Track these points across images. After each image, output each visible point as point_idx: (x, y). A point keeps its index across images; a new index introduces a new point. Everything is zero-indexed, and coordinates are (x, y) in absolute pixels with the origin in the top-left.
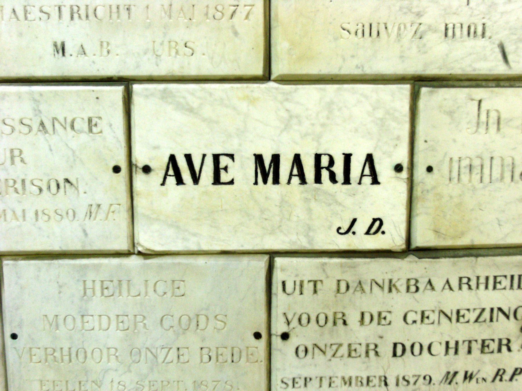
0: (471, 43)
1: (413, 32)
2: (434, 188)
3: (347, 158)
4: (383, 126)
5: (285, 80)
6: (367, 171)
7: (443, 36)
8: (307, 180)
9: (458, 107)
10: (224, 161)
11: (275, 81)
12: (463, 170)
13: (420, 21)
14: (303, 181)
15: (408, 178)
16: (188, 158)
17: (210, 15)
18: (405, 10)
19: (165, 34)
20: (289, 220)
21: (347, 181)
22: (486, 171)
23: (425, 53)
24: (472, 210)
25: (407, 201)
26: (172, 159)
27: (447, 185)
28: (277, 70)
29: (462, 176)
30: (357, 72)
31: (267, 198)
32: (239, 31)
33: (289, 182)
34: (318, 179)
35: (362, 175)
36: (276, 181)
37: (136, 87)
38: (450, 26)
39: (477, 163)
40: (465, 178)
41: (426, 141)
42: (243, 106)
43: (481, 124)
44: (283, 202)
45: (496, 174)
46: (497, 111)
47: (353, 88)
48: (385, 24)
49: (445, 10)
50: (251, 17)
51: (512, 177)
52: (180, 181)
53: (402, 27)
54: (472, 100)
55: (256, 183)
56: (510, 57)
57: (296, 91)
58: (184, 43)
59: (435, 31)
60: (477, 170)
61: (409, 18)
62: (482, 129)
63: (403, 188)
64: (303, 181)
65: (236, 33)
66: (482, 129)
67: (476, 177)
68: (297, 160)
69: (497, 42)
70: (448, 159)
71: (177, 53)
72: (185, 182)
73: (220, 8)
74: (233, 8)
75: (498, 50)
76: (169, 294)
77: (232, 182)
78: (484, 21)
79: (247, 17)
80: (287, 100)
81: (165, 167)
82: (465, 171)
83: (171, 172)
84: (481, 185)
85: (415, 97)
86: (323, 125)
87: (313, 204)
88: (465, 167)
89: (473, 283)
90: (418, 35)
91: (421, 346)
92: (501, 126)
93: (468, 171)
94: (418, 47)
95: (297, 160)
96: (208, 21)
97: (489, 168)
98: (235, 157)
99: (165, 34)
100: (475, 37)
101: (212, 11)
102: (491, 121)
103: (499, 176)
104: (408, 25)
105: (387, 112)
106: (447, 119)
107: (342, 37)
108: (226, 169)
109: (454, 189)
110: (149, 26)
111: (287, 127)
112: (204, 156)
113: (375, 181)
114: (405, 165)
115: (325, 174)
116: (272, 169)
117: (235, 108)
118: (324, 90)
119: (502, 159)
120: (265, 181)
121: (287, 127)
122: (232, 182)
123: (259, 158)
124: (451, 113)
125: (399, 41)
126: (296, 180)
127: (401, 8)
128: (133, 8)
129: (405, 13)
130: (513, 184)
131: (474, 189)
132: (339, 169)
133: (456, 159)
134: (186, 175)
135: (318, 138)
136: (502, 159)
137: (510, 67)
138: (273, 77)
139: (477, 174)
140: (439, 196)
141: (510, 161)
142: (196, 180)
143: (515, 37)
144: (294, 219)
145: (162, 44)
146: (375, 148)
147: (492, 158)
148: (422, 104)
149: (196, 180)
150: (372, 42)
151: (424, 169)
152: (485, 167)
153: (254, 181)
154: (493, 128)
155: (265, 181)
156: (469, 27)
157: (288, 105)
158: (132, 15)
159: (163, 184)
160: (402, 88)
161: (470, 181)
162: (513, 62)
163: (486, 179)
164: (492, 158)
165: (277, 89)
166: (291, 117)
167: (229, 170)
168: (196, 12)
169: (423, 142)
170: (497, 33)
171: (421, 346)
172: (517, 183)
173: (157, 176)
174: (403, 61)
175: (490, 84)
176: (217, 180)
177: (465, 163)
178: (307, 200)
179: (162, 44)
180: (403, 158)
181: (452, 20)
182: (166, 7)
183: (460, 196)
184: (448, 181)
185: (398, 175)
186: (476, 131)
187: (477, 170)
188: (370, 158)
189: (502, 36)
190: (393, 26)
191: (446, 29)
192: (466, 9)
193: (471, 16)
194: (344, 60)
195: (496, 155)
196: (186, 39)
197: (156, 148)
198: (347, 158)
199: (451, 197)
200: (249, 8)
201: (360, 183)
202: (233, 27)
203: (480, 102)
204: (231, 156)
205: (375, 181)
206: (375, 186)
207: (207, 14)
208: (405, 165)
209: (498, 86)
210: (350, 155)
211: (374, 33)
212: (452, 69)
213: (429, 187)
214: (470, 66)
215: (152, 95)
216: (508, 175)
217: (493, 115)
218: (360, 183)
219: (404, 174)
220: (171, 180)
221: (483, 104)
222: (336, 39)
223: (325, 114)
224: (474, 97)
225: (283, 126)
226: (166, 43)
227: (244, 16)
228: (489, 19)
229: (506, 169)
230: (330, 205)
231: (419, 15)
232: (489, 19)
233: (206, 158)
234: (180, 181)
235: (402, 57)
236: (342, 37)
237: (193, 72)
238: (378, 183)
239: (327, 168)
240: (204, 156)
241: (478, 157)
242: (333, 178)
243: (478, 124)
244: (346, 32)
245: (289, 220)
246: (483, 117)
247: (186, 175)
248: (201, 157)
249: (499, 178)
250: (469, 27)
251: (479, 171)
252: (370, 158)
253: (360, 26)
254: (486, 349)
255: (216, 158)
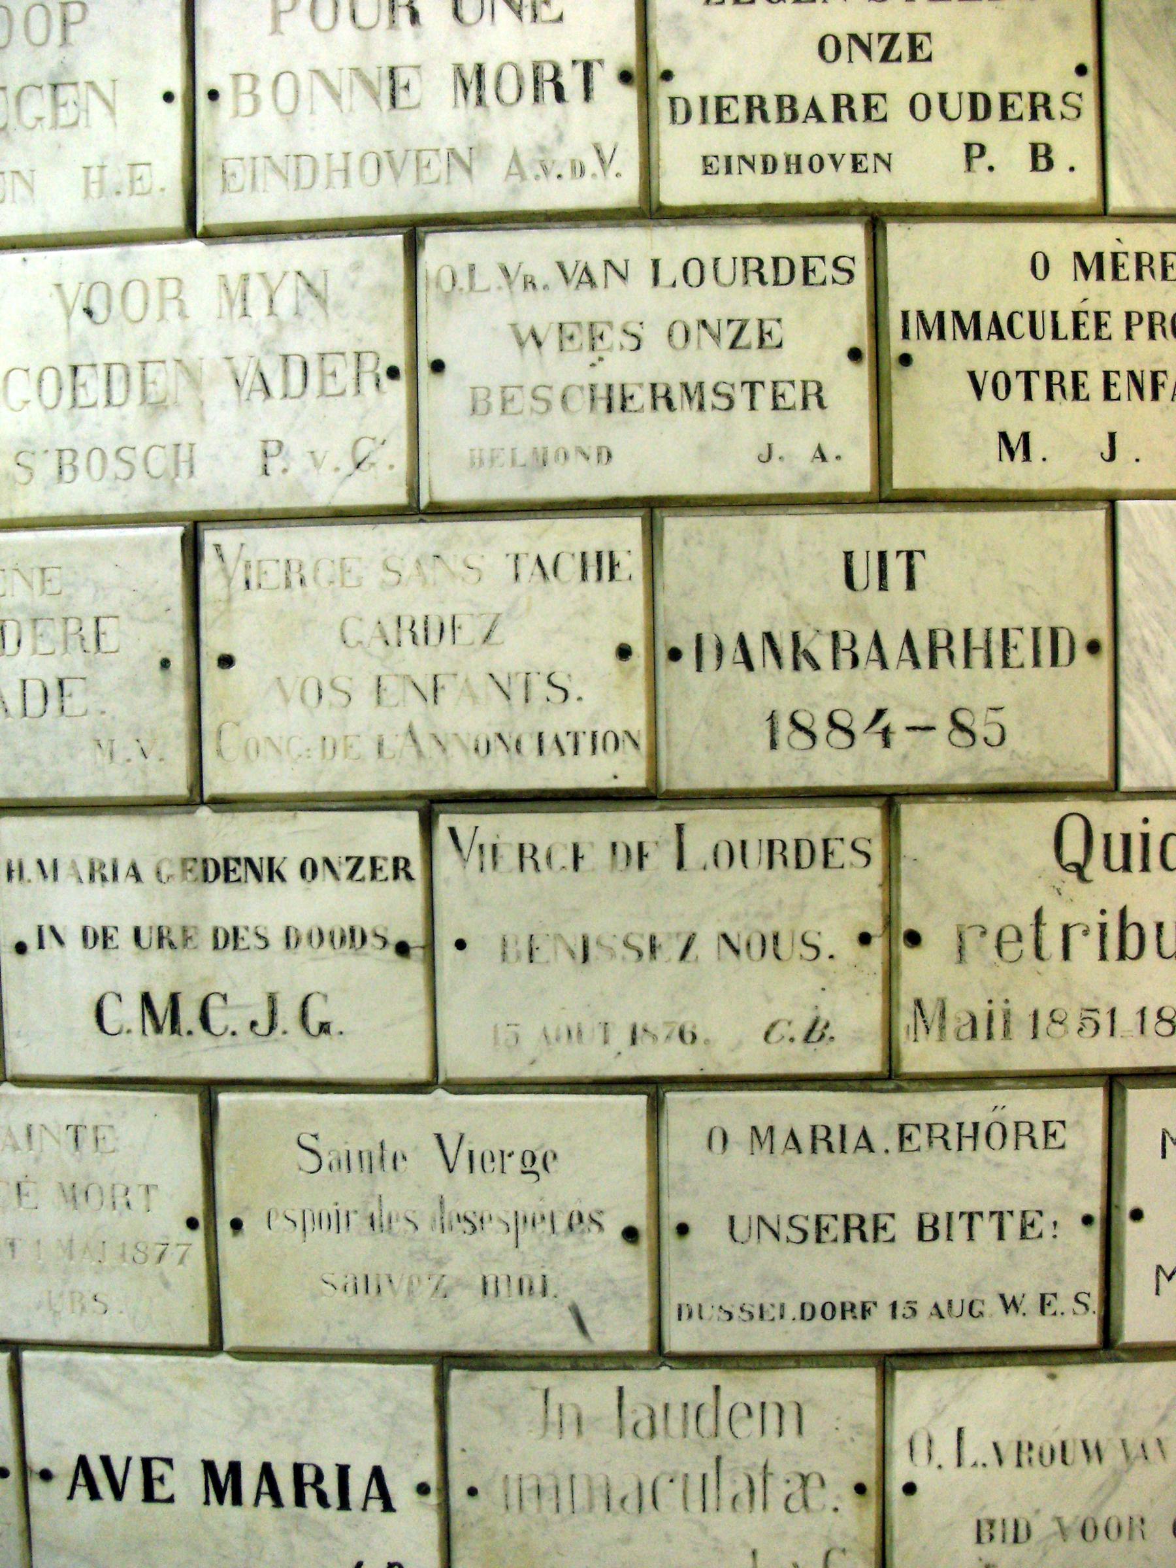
0: (526, 1305)
1: (433, 1288)
2: (481, 1519)
3: (343, 1472)
4: (394, 1425)
5: (242, 1354)
6: (374, 1491)
7: (481, 1294)
8: (284, 1501)
9: (512, 1400)
10: (158, 1469)
11: (229, 1352)
12: (525, 1494)
13: (442, 1272)
14: (278, 1502)
15: (439, 1504)
16: (106, 1461)
17: (128, 1258)
18: (419, 1256)
19: (65, 1282)
20: (259, 1559)
21: (344, 1504)
22: (565, 1495)
23: (453, 1318)
24: (546, 1554)
25: (440, 1539)
26: (83, 1461)
27: (502, 1516)
28: (233, 1337)
29: (526, 1503)
30: (350, 1346)
31: (225, 1526)
32: (172, 1280)
33: (256, 1503)
34: (300, 1501)
35: (367, 1498)
36: (237, 1500)
37: (27, 1356)
38: (491, 1280)
39: (548, 1483)
40: (530, 1505)
41: (463, 1450)
42: (183, 1390)
43: (550, 1426)
44: (250, 1532)
45: (581, 1498)
46: (576, 1406)
47: (345, 1369)
48: (389, 1276)
49: (481, 1255)
50: (186, 1260)
51: (608, 1504)
52: (95, 1495)
53: (415, 1281)
54: (533, 1389)
55: (207, 1502)
56: (588, 1326)
57: (258, 1370)
58: (92, 1295)
59: (468, 1286)
60: (549, 1494)
61: (425, 1267)
62: (553, 1433)
63: (431, 1521)
64: (278, 1502)
65: (166, 1284)
66: (553, 1433)
67: (548, 1505)
68: (267, 1471)
69: (568, 1303)
70: (500, 1478)
71: (83, 1308)
72: (102, 1494)
73: (141, 1247)
74: (162, 1248)
75: (568, 1315)
76: (48, 121)
77: (171, 1500)
78: (544, 1271)
79: (181, 1262)
80: (246, 1383)
81: (72, 1473)
82: (530, 1495)
83: (81, 1480)
84: (557, 1517)
85: (442, 1383)
86: (302, 1422)
87: (296, 1539)
88: (529, 1490)
89: (952, 1138)
90: (441, 1293)
91: (813, 1308)
92: (584, 1428)
93: (535, 1495)
94: (442, 1311)
95: (267, 1471)
96: (125, 1264)
97: (569, 1491)
98: (174, 1462)
99: (65, 1282)
100: (530, 1294)
101: (130, 1252)
102: (566, 1421)
103: (586, 1503)
104: (425, 1278)
105: (400, 1406)
106: (496, 1418)
107: (322, 1294)
108: (161, 1479)
109: (513, 1522)
110: (42, 1269)
111: (249, 1422)
112: (129, 1459)
113: (388, 1507)
114: (433, 1484)
115: (310, 1494)
116: (230, 1483)
117: (169, 1392)
118: (300, 1370)
119: (590, 1479)
120: (221, 1501)
121: (249, 1422)
122: (171, 1500)
123: (209, 1467)
124: (500, 1409)
125: (411, 1302)
126: (266, 1501)
127: (411, 1254)
128: (18, 1244)
129: (419, 1260)
130: (610, 1515)
131: (546, 1523)
132: (330, 1485)
133: (513, 1477)
134: (104, 1487)
135: (296, 1440)
136: (590, 1479)
137: (591, 1341)
138: (226, 1347)
139: (550, 1500)
140: (491, 1533)
141: (601, 1480)
142: (118, 1494)
143: (595, 1296)
144: (268, 1558)
145: (61, 1295)
146: (385, 1458)
147: (572, 1476)
148: (453, 1394)
149: (118, 1494)
150: (370, 1301)
151: (464, 1491)
152: (561, 1488)
153: (203, 1499)
154: (570, 1432)
155: (221, 1501)
156: (521, 1280)
157: (249, 1391)
158: (17, 1254)
159: (71, 1497)
160: (419, 1371)
161: (539, 1510)
162: (597, 1332)
163: (566, 1506)
164: (572, 1476)
165: (231, 1366)
166: (254, 1408)
167: (166, 1481)
168: (107, 1252)
169: (459, 1450)
170: (566, 1289)
171: (813, 1308)
172: (616, 1514)
173: (61, 1485)
174: (419, 1331)
175: (562, 1364)
176: (149, 1496)
177: (529, 1483)
178: (285, 1531)
179: (61, 1295)
180: (428, 1471)
181: (491, 1272)
182: (65, 1242)
183: (524, 1532)
184: (502, 1510)
185: (424, 1499)
186: (543, 1436)
187: (549, 1494)
188: (377, 1473)
189: (574, 1294)
190: (401, 1280)
191: (485, 1283)
192: (513, 1254)
193: (523, 1264)
194: (328, 1327)
195: (577, 1471)
196: (95, 1291)
197: (58, 1444)
198: (343, 1472)
199: (510, 1534)
200: (184, 1248)
201: (364, 1509)
202: (162, 1274)
203: (547, 1391)
204: (169, 1462)
205: (388, 1507)
206: (388, 1515)
207: (123, 1255)
208: (433, 1484)
209: (574, 1368)
210: (348, 1467)
211: (373, 1289)
212: (498, 1342)
213: (472, 1518)
214: (527, 1338)
215: (52, 1368)
216: (600, 1502)
217: (570, 1415)
218: (364, 1509)
219: (433, 1498)
220: (82, 1493)
221: (550, 1396)
222: (315, 1297)
223: (304, 1404)
224: (537, 1384)
225: (242, 1421)
226: (67, 1295)
227: (177, 1260)
228: (552, 1268)
229: (596, 1493)
230: (320, 1539)
231: (440, 1263)
232: (552, 1268)
233: (131, 1462)
234: (95, 1495)
235: (416, 1325)
236: (322, 1294)
237: (107, 1337)
238: (394, 1510)
239: (314, 1485)
240: (129, 1459)
241: (548, 1474)
242: (322, 1499)
243: (546, 1424)
244: (328, 1287)
245: (259, 1559)
246: (554, 1415)
247: (104, 1487)
248: (124, 1462)
249: (587, 1507)
250: (521, 1280)
251: (554, 1496)
252: (377, 1473)
253: (350, 1277)
254: (1051, 1139)
255: (147, 1463)
